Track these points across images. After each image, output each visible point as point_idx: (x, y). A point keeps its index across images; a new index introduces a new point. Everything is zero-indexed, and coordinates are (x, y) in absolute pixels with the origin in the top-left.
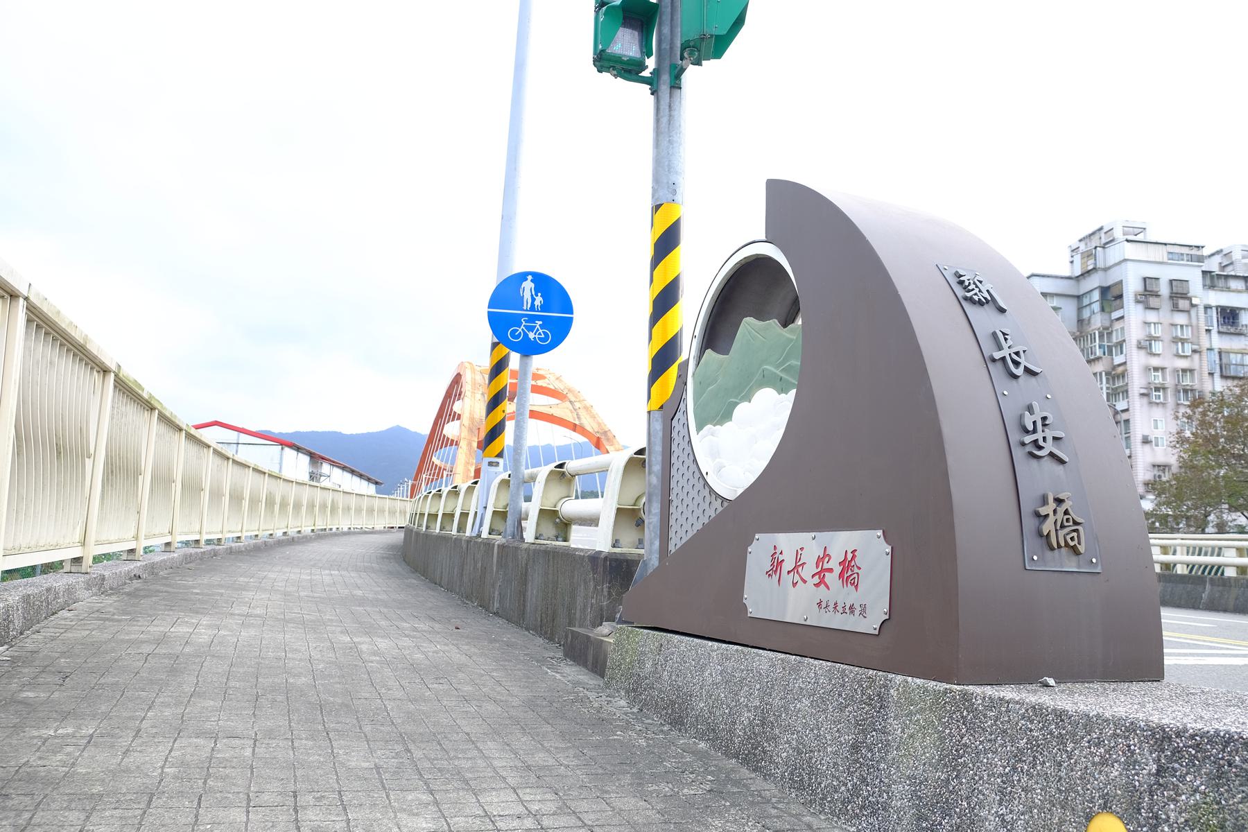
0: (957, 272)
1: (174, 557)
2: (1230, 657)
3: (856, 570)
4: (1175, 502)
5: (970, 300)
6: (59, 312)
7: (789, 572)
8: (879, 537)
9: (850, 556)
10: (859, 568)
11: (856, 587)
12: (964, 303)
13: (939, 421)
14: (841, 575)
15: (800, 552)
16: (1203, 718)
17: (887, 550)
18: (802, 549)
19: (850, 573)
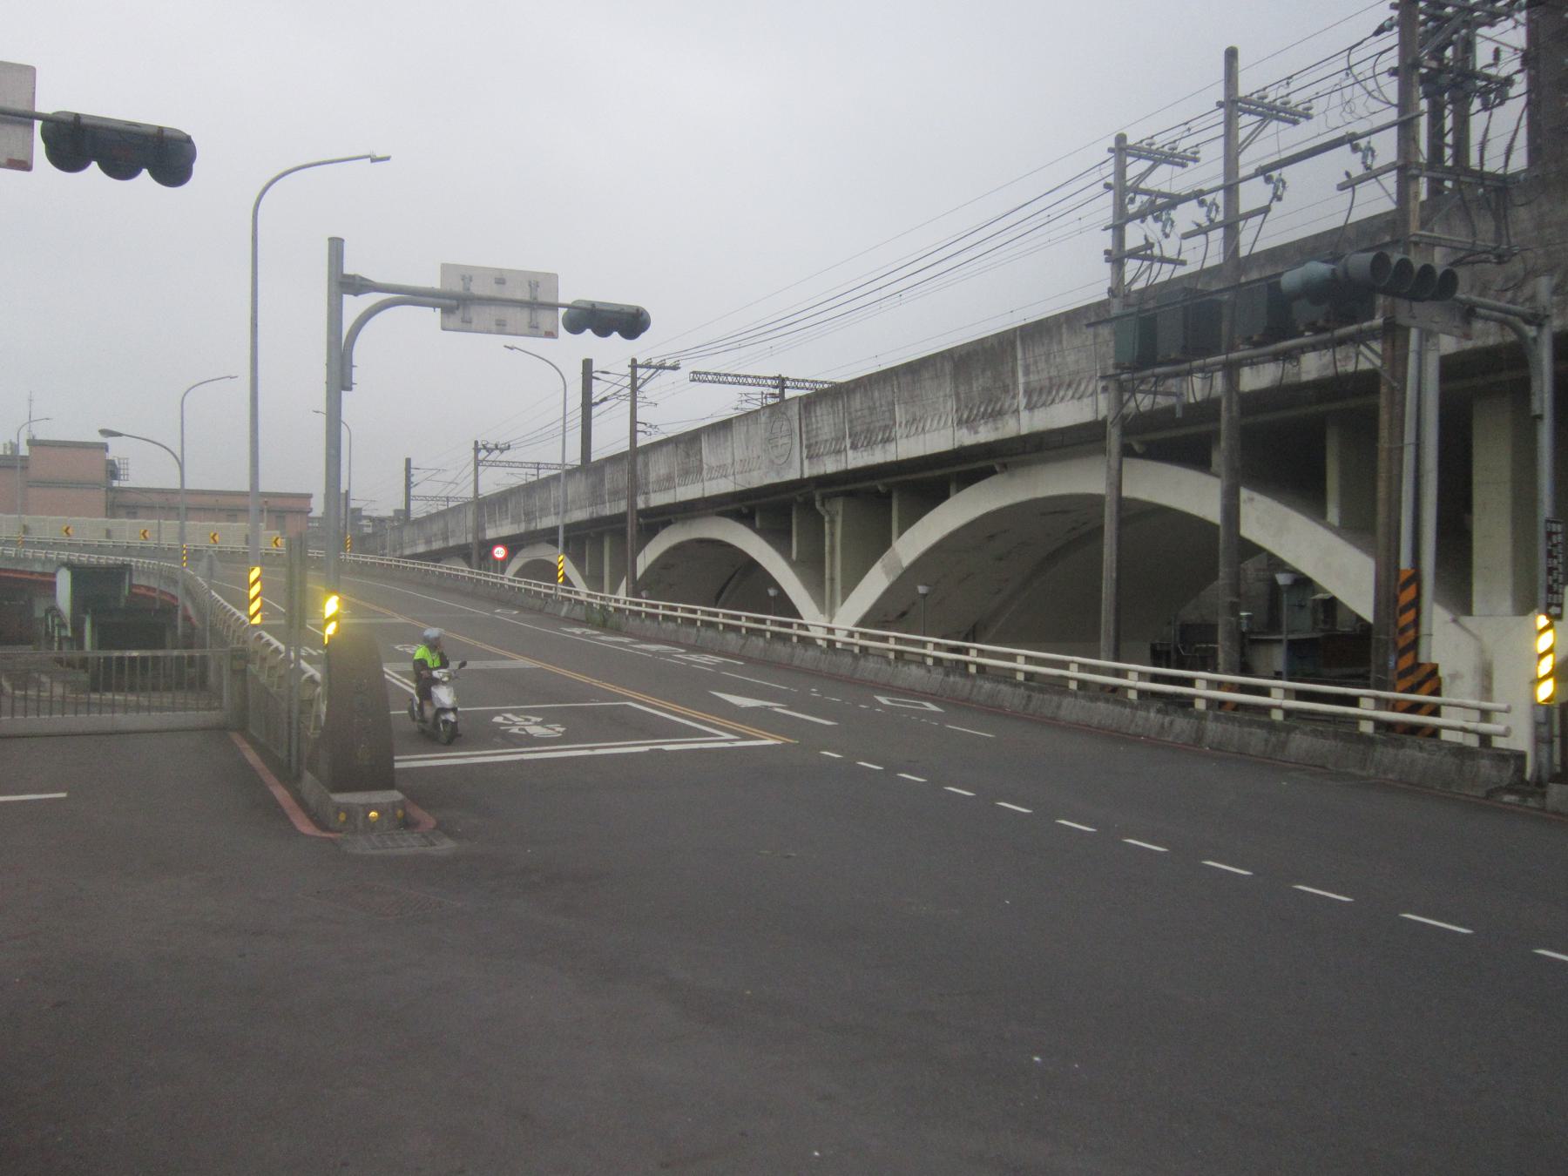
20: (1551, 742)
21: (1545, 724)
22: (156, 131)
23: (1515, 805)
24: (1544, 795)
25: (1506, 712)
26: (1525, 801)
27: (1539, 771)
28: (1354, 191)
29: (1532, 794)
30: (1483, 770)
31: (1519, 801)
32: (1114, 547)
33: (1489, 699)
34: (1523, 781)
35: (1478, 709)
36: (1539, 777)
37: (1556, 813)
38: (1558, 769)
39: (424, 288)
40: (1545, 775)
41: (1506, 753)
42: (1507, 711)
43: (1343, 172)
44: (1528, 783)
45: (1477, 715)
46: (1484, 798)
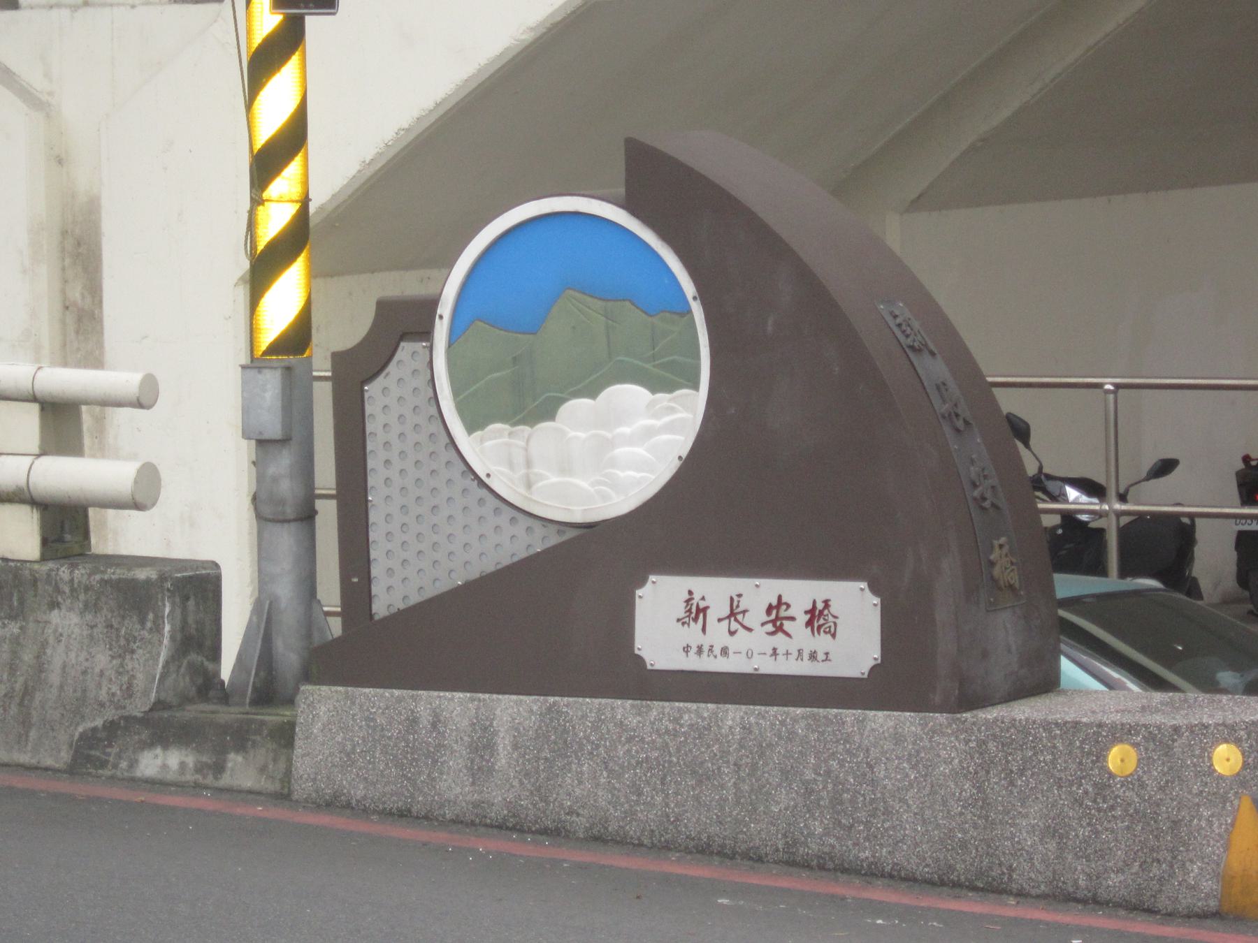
0: (892, 311)
1: (94, 729)
2: (1079, 388)
3: (831, 619)
4: (1191, 763)
5: (912, 347)
6: (248, 509)
7: (720, 620)
8: (862, 590)
9: (820, 606)
10: (835, 617)
11: (834, 636)
12: (907, 350)
13: (681, 260)
14: (809, 623)
15: (736, 599)
16: (101, 689)
17: (875, 602)
18: (740, 596)
19: (822, 621)
20: (307, 516)
21: (284, 441)
22: (1160, 462)
23: (179, 786)
24: (285, 736)
25: (139, 404)
26: (219, 768)
27: (267, 639)
28: (744, 615)
29: (240, 738)
30: (57, 657)
31: (200, 769)
32: (1205, 384)
33: (95, 360)
34: (208, 685)
35: (33, 398)
36: (267, 659)
37: (334, 804)
38: (336, 627)
39: (283, 125)
40: (289, 656)
41: (142, 574)
42: (143, 402)
43: (748, 608)
44: (225, 696)
45: (28, 421)
46: (72, 770)
